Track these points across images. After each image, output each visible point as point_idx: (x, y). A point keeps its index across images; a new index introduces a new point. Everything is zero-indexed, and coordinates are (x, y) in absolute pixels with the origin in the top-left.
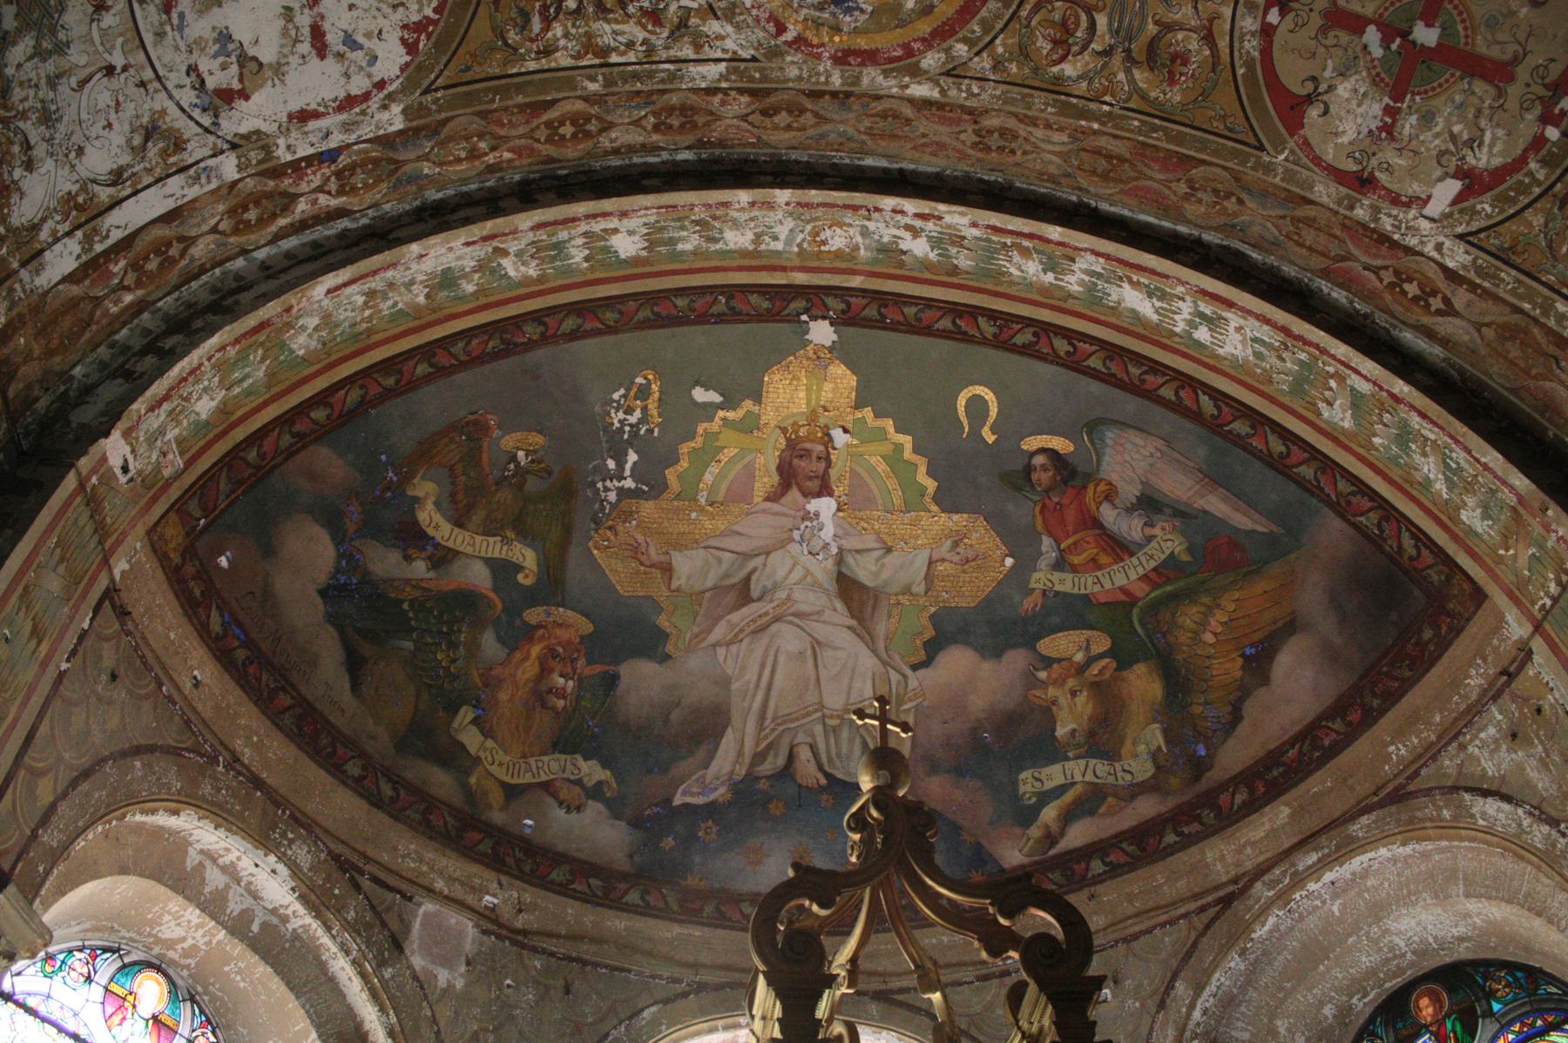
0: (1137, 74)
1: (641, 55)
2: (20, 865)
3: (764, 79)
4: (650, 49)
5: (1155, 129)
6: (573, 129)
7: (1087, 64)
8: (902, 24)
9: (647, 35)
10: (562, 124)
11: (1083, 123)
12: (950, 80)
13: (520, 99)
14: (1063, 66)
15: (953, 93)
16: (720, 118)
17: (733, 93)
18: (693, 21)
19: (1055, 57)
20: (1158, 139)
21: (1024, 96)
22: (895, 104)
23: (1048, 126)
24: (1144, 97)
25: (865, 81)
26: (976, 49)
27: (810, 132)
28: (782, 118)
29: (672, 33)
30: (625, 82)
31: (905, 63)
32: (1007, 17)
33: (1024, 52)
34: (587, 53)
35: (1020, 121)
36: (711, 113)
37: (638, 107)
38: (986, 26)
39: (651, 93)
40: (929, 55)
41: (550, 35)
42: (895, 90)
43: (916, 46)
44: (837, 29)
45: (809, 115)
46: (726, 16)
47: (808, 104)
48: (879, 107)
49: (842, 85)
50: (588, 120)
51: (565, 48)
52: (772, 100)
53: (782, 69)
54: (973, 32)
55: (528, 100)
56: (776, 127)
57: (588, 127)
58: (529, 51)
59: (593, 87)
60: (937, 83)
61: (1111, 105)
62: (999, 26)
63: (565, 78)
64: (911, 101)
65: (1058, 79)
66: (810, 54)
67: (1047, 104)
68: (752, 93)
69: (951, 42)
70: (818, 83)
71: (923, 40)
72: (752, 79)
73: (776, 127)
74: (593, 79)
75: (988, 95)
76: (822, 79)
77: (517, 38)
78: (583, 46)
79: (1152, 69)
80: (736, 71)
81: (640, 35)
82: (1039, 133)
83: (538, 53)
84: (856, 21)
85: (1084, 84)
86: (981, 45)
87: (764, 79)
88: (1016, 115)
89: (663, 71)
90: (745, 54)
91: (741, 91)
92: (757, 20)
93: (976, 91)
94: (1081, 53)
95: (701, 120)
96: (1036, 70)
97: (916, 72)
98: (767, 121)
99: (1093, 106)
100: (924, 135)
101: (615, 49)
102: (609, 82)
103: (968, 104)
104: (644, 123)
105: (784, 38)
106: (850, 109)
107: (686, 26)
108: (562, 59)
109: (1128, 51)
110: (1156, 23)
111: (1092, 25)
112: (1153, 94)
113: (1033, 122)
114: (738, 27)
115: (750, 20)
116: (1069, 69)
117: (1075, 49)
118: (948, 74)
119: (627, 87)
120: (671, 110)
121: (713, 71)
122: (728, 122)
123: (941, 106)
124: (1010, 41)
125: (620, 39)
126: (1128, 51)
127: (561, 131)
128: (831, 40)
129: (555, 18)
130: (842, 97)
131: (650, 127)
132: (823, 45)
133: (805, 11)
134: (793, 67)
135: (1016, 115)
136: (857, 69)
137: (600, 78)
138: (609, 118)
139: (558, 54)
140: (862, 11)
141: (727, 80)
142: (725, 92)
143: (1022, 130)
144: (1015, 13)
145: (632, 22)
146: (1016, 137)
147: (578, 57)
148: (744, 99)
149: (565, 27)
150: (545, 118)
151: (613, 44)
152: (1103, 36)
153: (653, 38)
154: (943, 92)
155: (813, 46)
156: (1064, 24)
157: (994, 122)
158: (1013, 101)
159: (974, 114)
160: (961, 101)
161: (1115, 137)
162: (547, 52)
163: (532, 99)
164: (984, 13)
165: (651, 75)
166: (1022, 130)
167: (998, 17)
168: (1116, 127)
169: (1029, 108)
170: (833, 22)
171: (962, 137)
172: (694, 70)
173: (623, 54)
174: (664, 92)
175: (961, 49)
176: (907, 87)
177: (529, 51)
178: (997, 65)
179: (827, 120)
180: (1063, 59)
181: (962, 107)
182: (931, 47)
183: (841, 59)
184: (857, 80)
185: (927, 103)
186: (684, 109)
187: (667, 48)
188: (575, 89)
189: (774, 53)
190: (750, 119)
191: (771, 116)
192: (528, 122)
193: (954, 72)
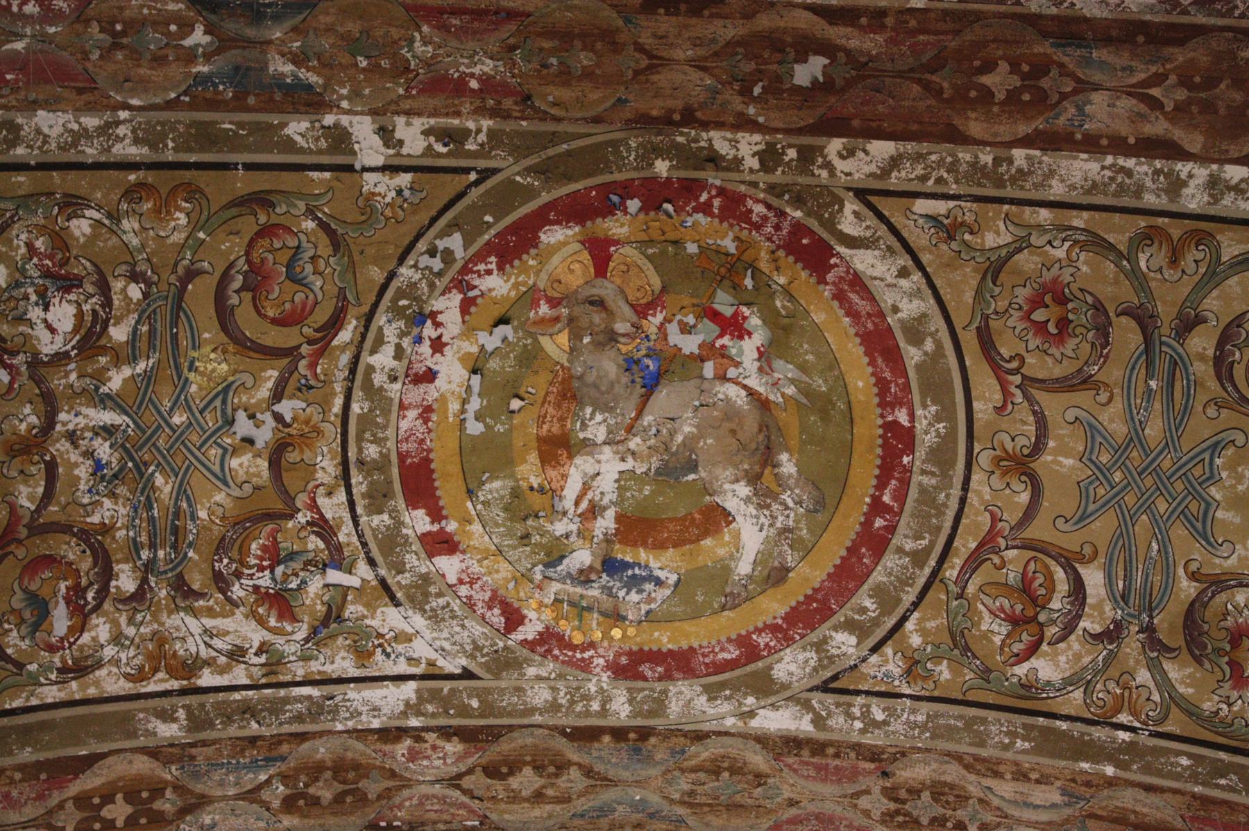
0: (1174, 671)
1: (257, 672)
2: (327, 175)
3: (488, 709)
4: (275, 662)
5: (1221, 770)
6: (129, 810)
7: (1077, 657)
8: (733, 602)
9: (268, 637)
10: (108, 799)
11: (1085, 766)
12: (830, 699)
13: (27, 755)
14: (1034, 662)
15: (837, 721)
16: (407, 783)
17: (431, 737)
18: (353, 609)
19: (1017, 647)
20: (1231, 789)
21: (970, 723)
22: (732, 747)
23: (1021, 776)
24: (1191, 711)
25: (674, 707)
26: (871, 642)
27: (581, 805)
28: (526, 780)
29: (314, 631)
30: (229, 720)
31: (745, 669)
32: (922, 581)
33: (960, 643)
34: (156, 670)
35: (968, 767)
36: (393, 774)
37: (254, 766)
38: (885, 598)
39: (278, 740)
40: (788, 654)
41: (86, 638)
42: (730, 722)
43: (762, 640)
44: (616, 617)
45: (574, 773)
46: (411, 599)
47: (572, 752)
48: (703, 753)
49: (634, 714)
50: (158, 791)
51: (115, 662)
52: (505, 747)
53: (519, 690)
54: (864, 610)
55: (42, 756)
56: (515, 798)
57: (157, 805)
58: (45, 668)
59: (168, 731)
60: (807, 706)
61: (1132, 729)
62: (909, 597)
63: (115, 715)
64: (762, 740)
65: (1029, 687)
66: (570, 663)
67: (1013, 735)
68: (468, 735)
69: (824, 630)
70: (587, 713)
71: (774, 629)
72: (465, 711)
73: (515, 798)
74: (167, 716)
75: (902, 724)
76: (595, 706)
77: (24, 645)
78: (150, 657)
79: (1198, 660)
80: (435, 695)
81: (255, 636)
82: (1005, 789)
83: (63, 670)
84: (650, 600)
85: (1078, 694)
86: (880, 633)
87: (488, 709)
88: (958, 758)
89: (299, 699)
90: (451, 666)
91: (447, 733)
92: (470, 604)
93: (879, 716)
94: (1063, 638)
95: (372, 787)
96: (985, 673)
97: (765, 687)
98: (498, 787)
99: (1099, 733)
100: (792, 803)
101: (209, 663)
102: (197, 722)
103: (867, 740)
104: (265, 795)
105: (518, 635)
106: (649, 760)
107: (339, 619)
108: (110, 682)
109: (1149, 629)
110: (1193, 576)
111: (1078, 589)
112: (1208, 706)
113: (992, 769)
114: (435, 618)
115: (456, 605)
116: (1046, 668)
117: (1051, 631)
118: (825, 688)
119: (233, 731)
120: (315, 771)
121: (391, 700)
122: (425, 789)
123: (818, 748)
124: (931, 625)
125: (218, 643)
126: (1149, 629)
127: (106, 812)
128: (606, 635)
129: (97, 608)
130: (633, 738)
131: (276, 804)
132: (592, 645)
133: (555, 587)
134: (539, 687)
135: (958, 758)
136: (659, 686)
137: (181, 714)
138: (199, 788)
139: (102, 673)
140: (659, 583)
141: (419, 713)
142: (417, 735)
143: (973, 785)
144: (935, 574)
145: (240, 612)
146: (963, 798)
147: (139, 676)
148: (453, 747)
149: (115, 623)
150: (74, 788)
151: (204, 653)
152: (1099, 606)
153: (280, 640)
154: (818, 721)
155: (574, 648)
156: (1025, 589)
157: (916, 772)
158: (949, 733)
159: (881, 760)
160: (855, 738)
161: (1149, 788)
162: (81, 668)
163: (50, 755)
164: (878, 576)
165: (276, 707)
166: (973, 785)
167: (906, 582)
168: (1147, 770)
169: (982, 744)
170: (607, 604)
171: (864, 802)
172: (354, 694)
173: (222, 671)
174: (302, 737)
175: (844, 643)
176: (752, 714)
177: (45, 668)
178: (913, 668)
179: (609, 782)
180: (1033, 650)
181: (857, 747)
182: (789, 641)
183: (628, 667)
184: (660, 706)
185: (791, 744)
186: (339, 768)
187: (305, 658)
188: (133, 735)
189: (503, 663)
190: (467, 782)
191: (503, 777)
192: (41, 797)
193: (833, 685)
